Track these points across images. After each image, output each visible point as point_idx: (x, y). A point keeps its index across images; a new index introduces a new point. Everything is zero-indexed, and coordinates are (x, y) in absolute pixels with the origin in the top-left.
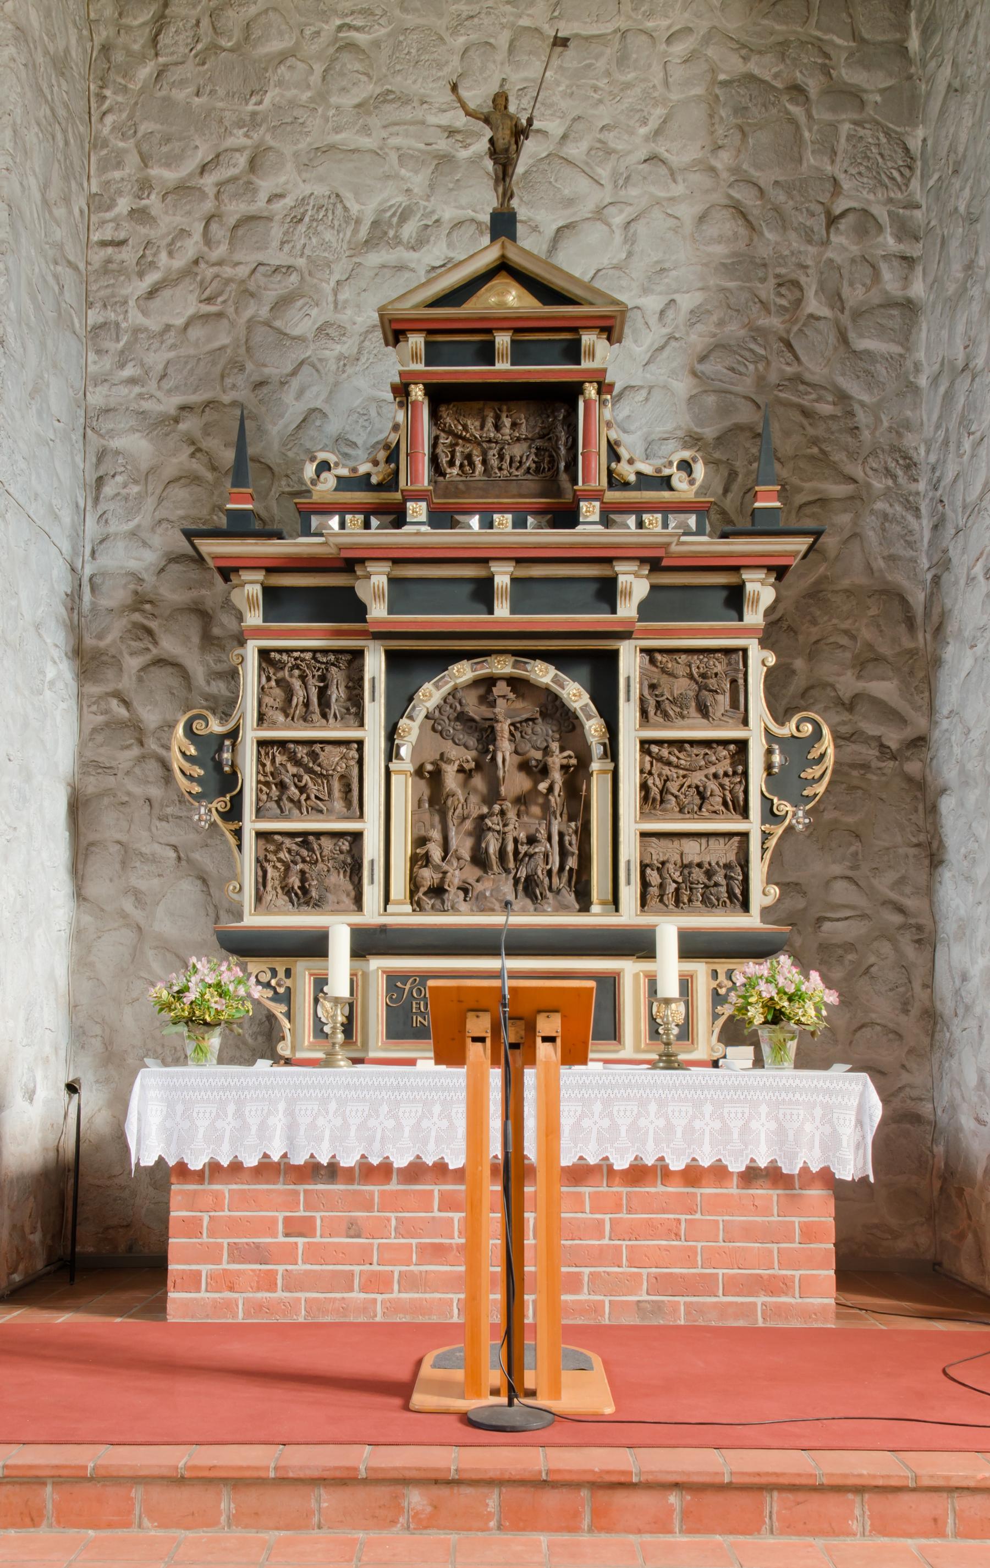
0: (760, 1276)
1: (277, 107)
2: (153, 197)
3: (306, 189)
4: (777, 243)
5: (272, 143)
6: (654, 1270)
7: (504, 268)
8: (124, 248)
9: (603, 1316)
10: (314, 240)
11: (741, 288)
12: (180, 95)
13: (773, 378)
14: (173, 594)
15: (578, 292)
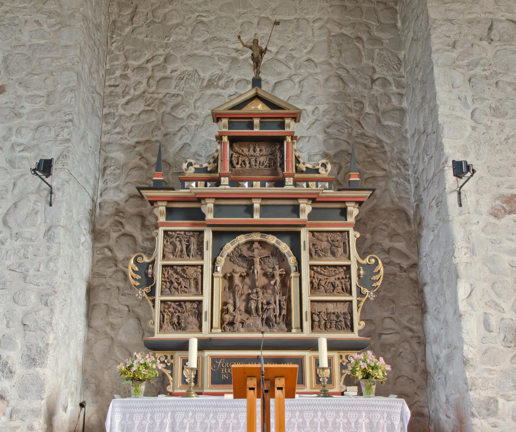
1: (175, 42)
2: (129, 70)
4: (354, 89)
7: (257, 97)
8: (118, 88)
10: (187, 86)
11: (342, 104)
12: (140, 37)
13: (354, 134)
14: (130, 209)
15: (283, 105)
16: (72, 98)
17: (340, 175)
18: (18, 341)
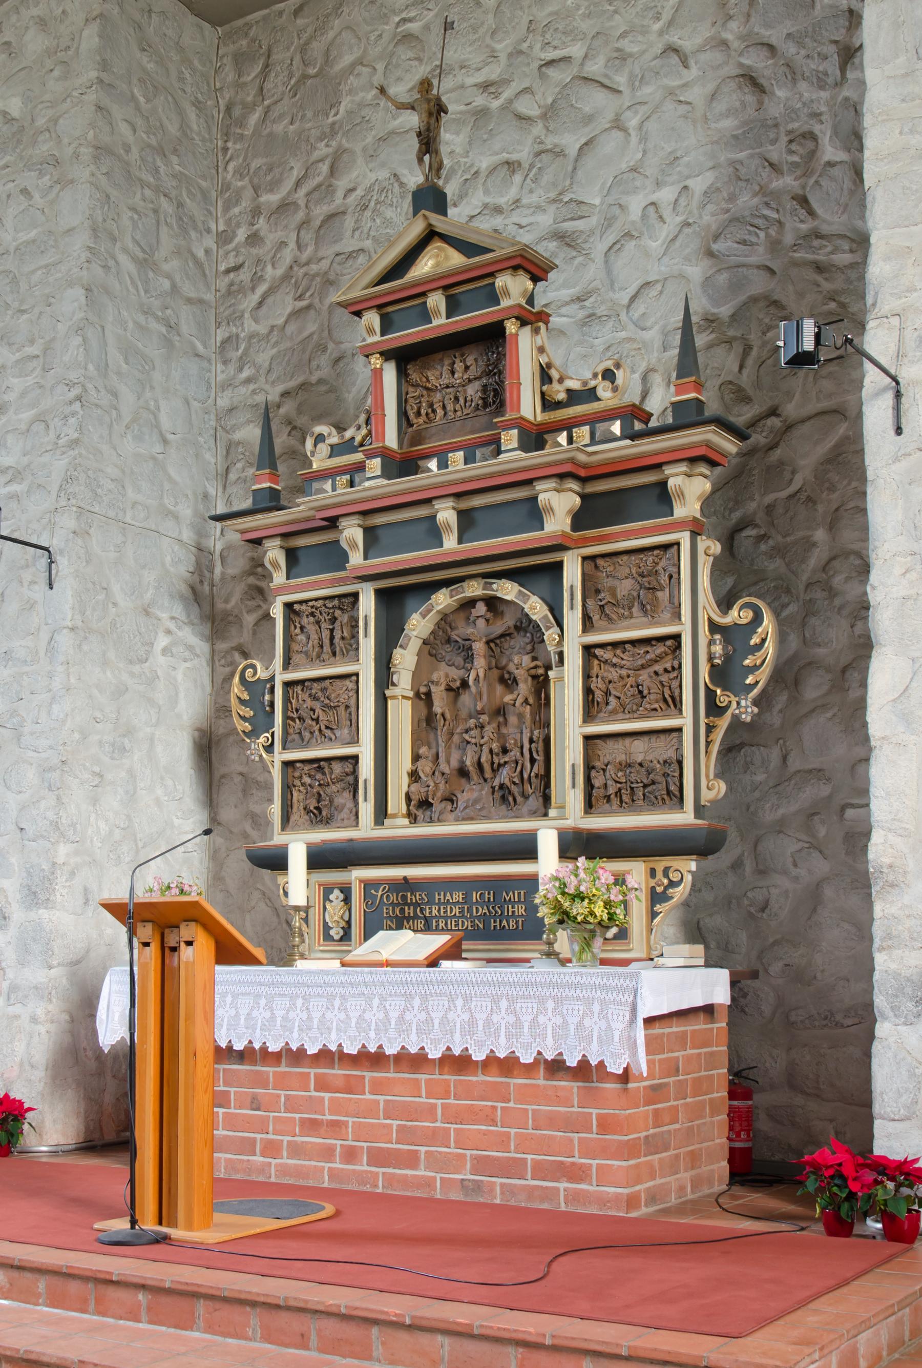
0: (562, 1162)
1: (350, 113)
2: (261, 221)
3: (372, 177)
4: (787, 99)
5: (347, 145)
6: (475, 1152)
7: (430, 235)
8: (241, 271)
9: (435, 1190)
10: (378, 221)
11: (751, 156)
12: (279, 128)
13: (789, 238)
15: (486, 242)
16: (79, 346)
17: (745, 372)
18: (13, 860)
